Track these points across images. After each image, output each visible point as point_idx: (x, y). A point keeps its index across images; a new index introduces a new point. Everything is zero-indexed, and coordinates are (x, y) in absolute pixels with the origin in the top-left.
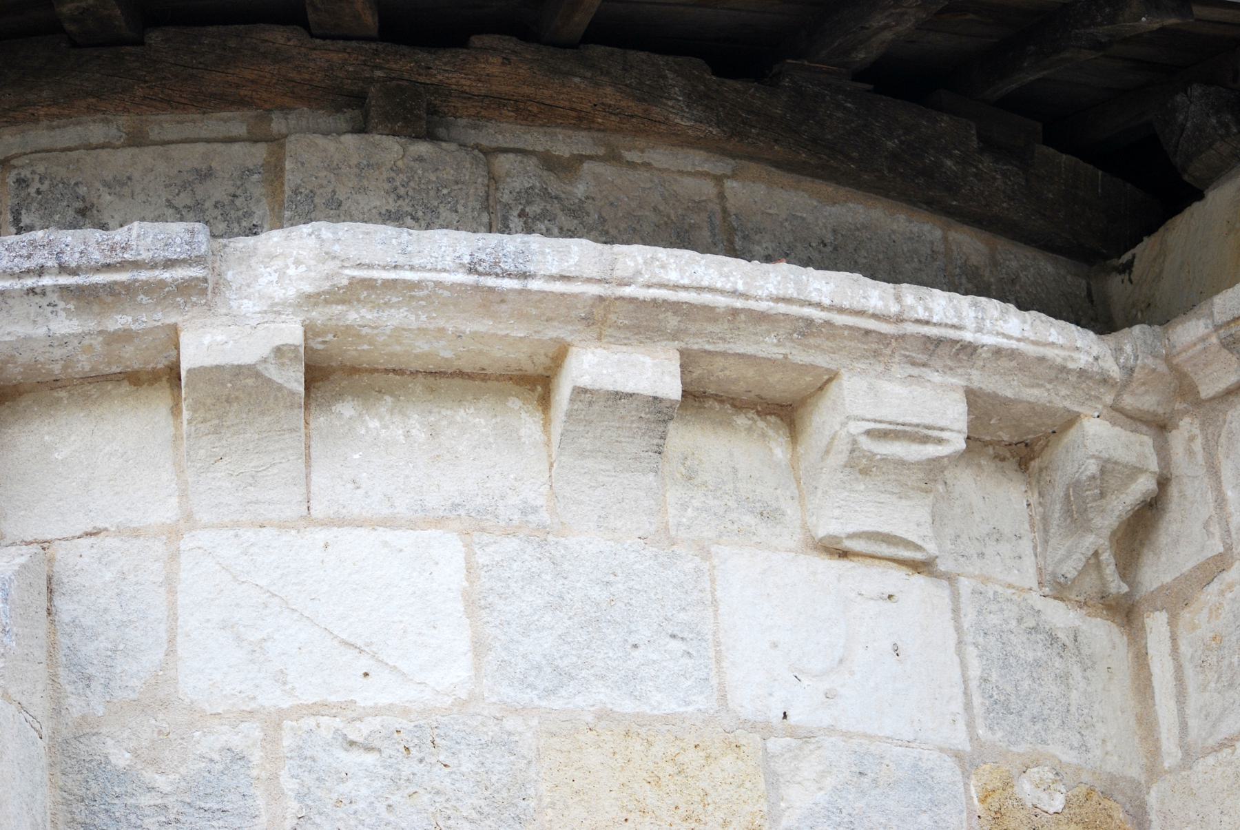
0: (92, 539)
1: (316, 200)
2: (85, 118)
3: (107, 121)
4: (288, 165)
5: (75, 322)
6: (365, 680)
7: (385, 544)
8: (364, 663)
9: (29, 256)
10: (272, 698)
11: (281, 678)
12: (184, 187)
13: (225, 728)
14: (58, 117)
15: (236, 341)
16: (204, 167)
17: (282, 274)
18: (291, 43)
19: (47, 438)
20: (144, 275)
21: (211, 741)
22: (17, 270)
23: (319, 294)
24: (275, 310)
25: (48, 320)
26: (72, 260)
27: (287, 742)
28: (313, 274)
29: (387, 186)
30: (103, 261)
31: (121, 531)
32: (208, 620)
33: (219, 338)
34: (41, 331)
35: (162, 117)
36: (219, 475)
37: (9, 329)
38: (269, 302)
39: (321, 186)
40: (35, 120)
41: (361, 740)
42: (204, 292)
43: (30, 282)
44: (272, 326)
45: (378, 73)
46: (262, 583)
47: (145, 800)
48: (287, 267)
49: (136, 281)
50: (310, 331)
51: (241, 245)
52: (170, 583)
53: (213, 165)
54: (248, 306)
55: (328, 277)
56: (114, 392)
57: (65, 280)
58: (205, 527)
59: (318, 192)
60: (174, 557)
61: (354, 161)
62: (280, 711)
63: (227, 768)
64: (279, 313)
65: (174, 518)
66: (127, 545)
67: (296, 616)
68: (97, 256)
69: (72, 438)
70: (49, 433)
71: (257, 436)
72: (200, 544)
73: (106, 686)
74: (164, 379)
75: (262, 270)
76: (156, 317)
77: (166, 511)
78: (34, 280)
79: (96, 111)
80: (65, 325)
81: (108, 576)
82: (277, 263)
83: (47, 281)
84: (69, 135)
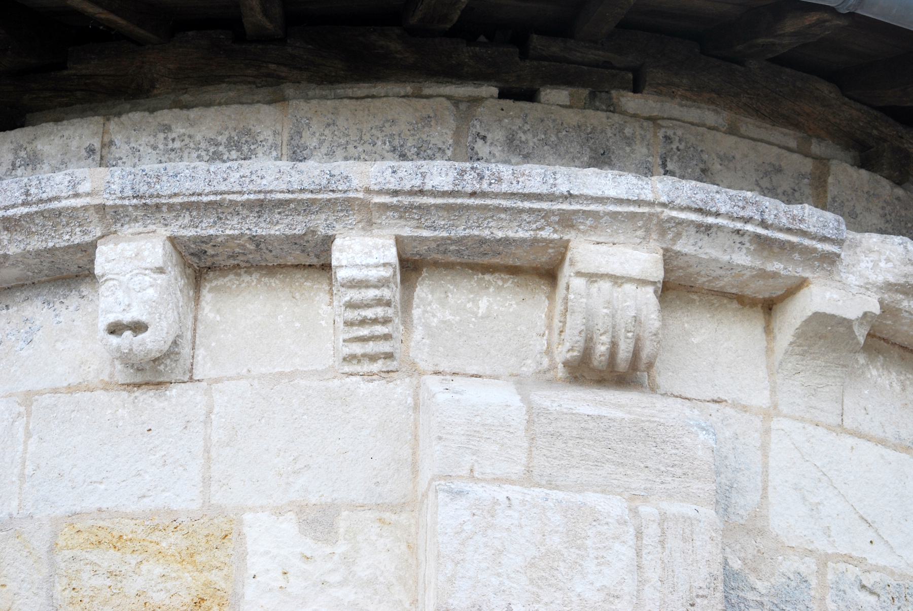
0: (717, 406)
1: (845, 209)
2: (703, 105)
3: (717, 112)
4: (830, 180)
5: (749, 258)
6: (869, 544)
7: (882, 456)
8: (871, 534)
9: (743, 208)
10: (821, 545)
11: (827, 531)
12: (766, 174)
13: (796, 558)
14: (687, 98)
15: (844, 301)
16: (777, 164)
17: (876, 264)
18: (832, 95)
19: (686, 325)
20: (807, 242)
21: (790, 564)
22: (735, 215)
23: (896, 285)
24: (867, 287)
25: (733, 252)
26: (770, 219)
27: (830, 577)
28: (896, 271)
29: (881, 212)
30: (788, 225)
31: (735, 405)
32: (786, 481)
33: (835, 296)
34: (726, 258)
35: (748, 120)
36: (796, 383)
37: (707, 251)
38: (866, 281)
39: (848, 200)
40: (673, 96)
41: (869, 586)
42: (833, 263)
43: (739, 225)
44: (864, 297)
45: (875, 132)
46: (818, 464)
47: (750, 596)
48: (880, 261)
49: (802, 244)
50: (886, 309)
51: (851, 236)
52: (764, 448)
53: (782, 164)
54: (852, 279)
55: (905, 276)
56: (729, 306)
57: (760, 231)
58: (785, 416)
59: (847, 204)
60: (767, 431)
61: (866, 190)
62: (827, 554)
63: (798, 586)
64: (868, 289)
65: (768, 405)
66: (739, 416)
67: (836, 492)
68: (784, 220)
69: (703, 331)
70: (687, 322)
71: (823, 364)
72: (783, 427)
73: (726, 510)
74: (760, 306)
75: (863, 257)
76: (798, 270)
77: (762, 399)
78: (742, 224)
79: (713, 103)
80: (742, 259)
81: (727, 434)
82: (874, 256)
83: (750, 228)
84: (693, 114)
